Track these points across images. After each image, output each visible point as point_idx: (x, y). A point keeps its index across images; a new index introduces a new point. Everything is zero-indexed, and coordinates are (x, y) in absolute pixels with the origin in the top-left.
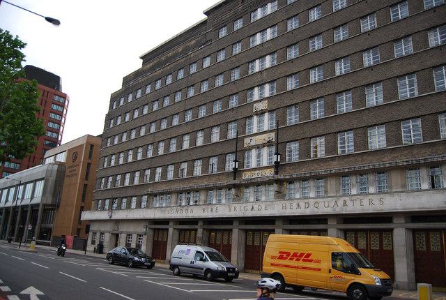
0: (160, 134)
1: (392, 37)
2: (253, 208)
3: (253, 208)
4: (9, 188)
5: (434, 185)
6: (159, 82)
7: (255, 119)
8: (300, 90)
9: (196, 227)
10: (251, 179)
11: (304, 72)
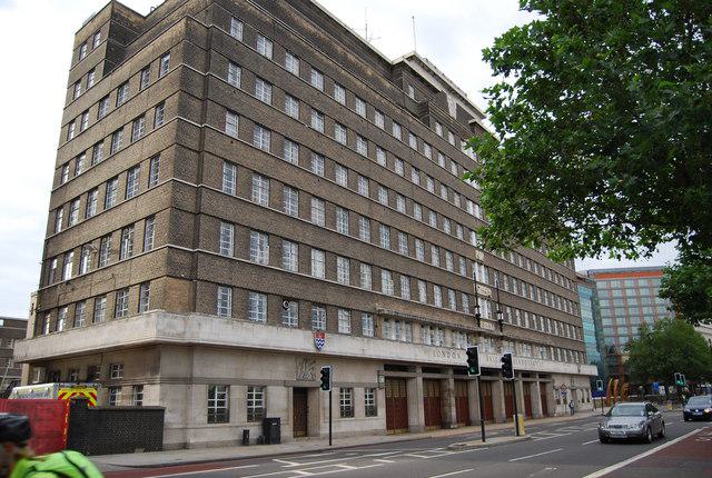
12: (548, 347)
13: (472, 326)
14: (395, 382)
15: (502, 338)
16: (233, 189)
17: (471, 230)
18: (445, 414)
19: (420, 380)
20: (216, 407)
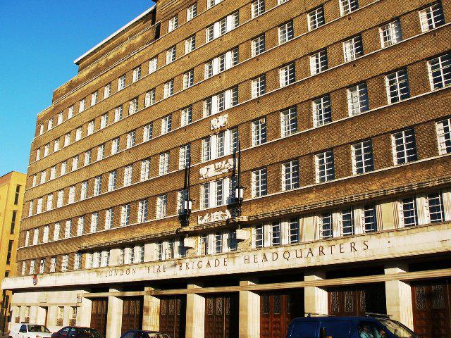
0: (97, 167)
1: (377, 21)
2: (209, 263)
3: (209, 263)
4: (210, 61)
5: (437, 216)
6: (94, 97)
7: (214, 140)
9: (142, 293)
10: (208, 224)
11: (272, 72)
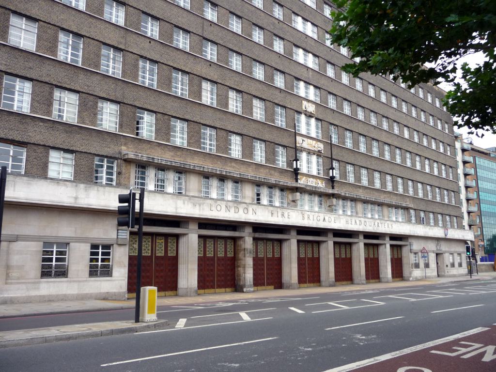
8: (86, 17)
12: (407, 209)
13: (291, 183)
14: (310, 246)
15: (333, 195)
16: (155, 83)
17: (298, 79)
18: (239, 275)
19: (388, 246)
20: (100, 263)
